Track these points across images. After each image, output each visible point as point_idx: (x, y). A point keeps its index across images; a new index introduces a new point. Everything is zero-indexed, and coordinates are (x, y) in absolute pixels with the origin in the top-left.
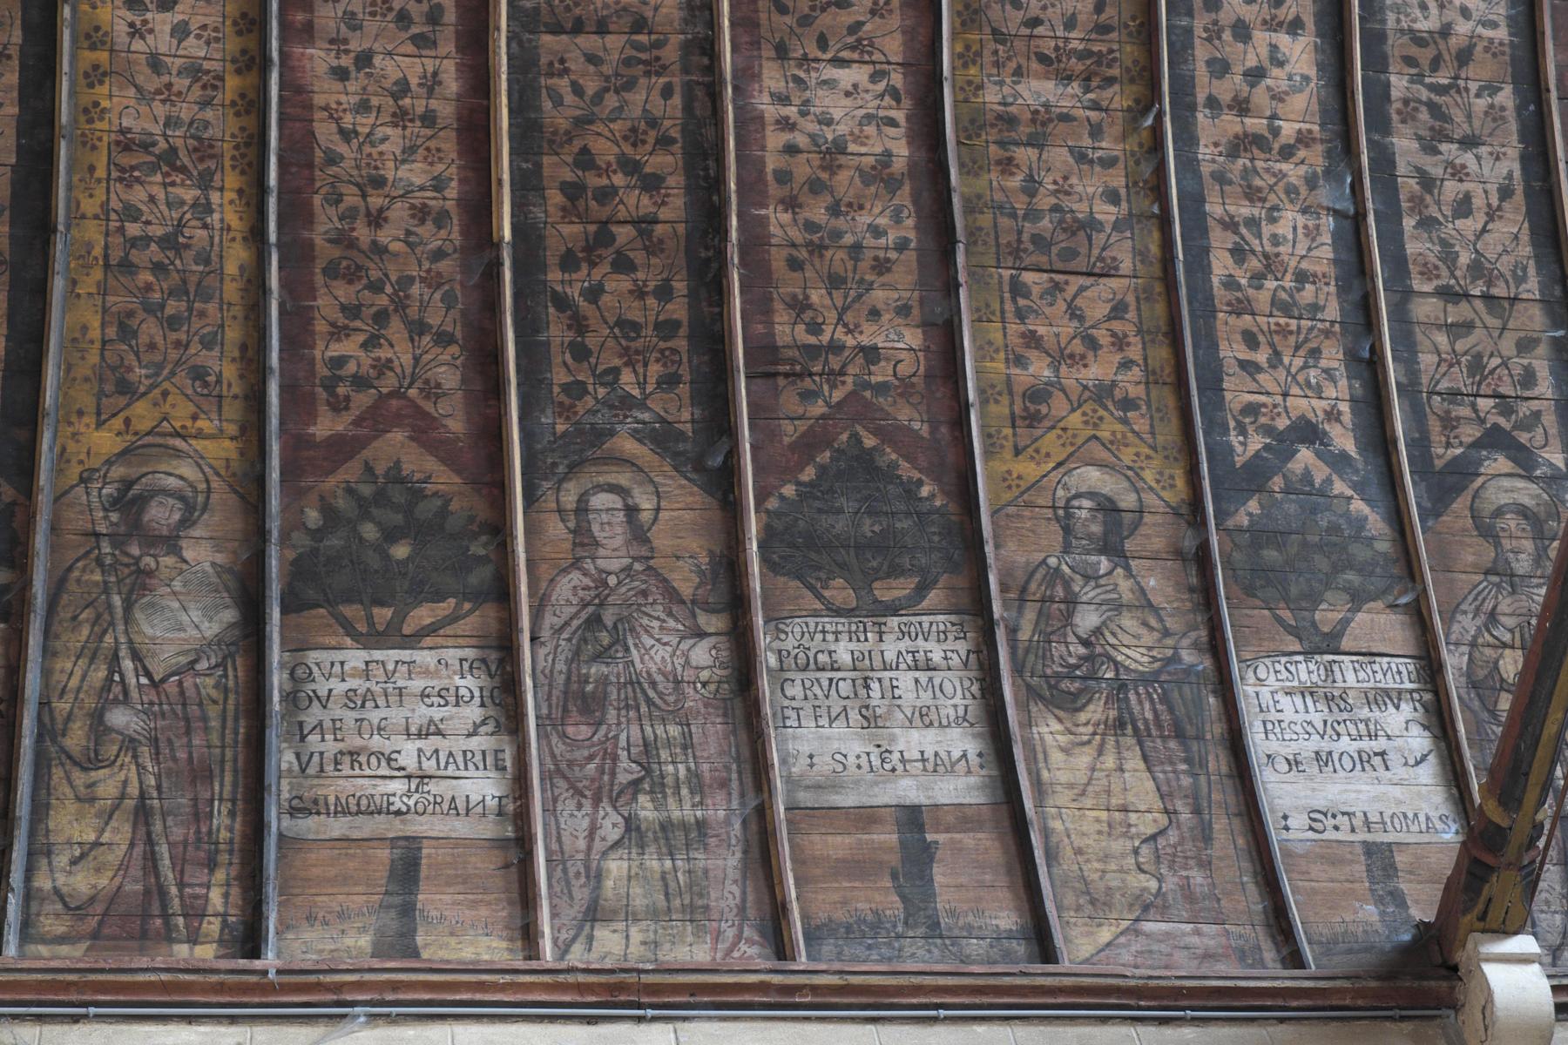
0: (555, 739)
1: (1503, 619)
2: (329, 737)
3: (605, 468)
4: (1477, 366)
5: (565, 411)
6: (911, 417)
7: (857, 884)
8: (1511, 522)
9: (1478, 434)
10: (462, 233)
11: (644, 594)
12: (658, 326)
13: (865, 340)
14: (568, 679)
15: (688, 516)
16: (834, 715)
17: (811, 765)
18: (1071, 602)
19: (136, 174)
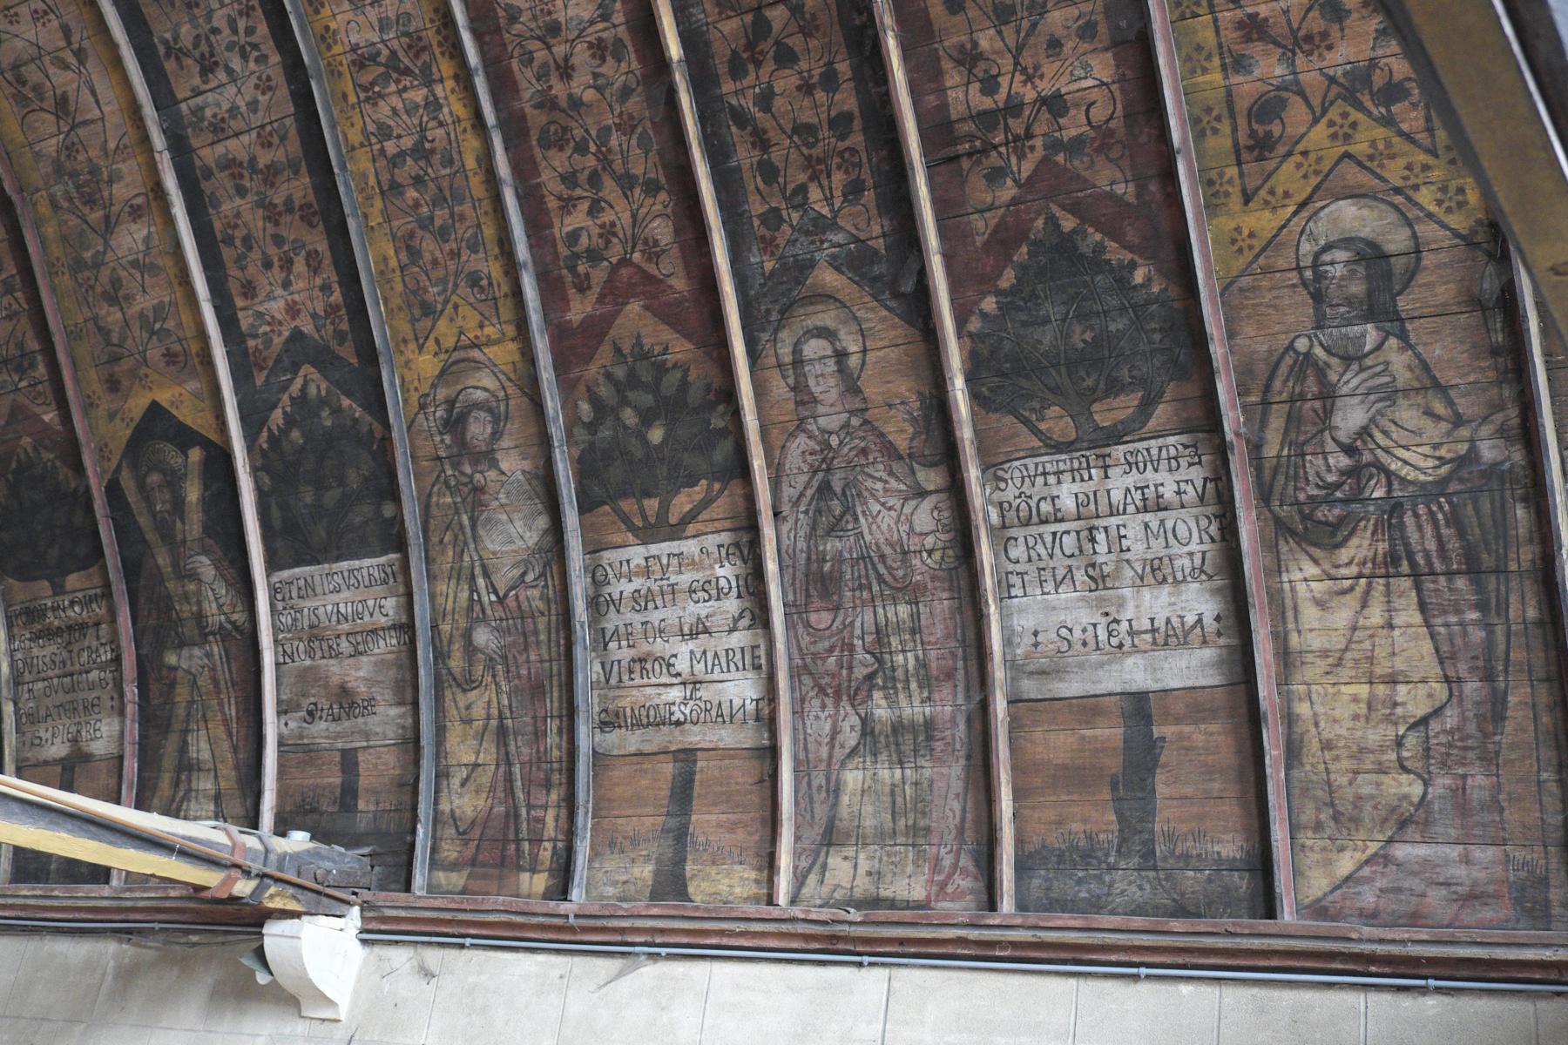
0: (801, 630)
2: (624, 643)
3: (811, 309)
5: (768, 245)
6: (1113, 180)
7: (1075, 797)
10: (639, 60)
11: (864, 452)
12: (832, 123)
13: (1045, 87)
14: (809, 558)
15: (893, 354)
16: (1059, 578)
17: (1036, 645)
18: (1328, 396)
19: (377, 89)
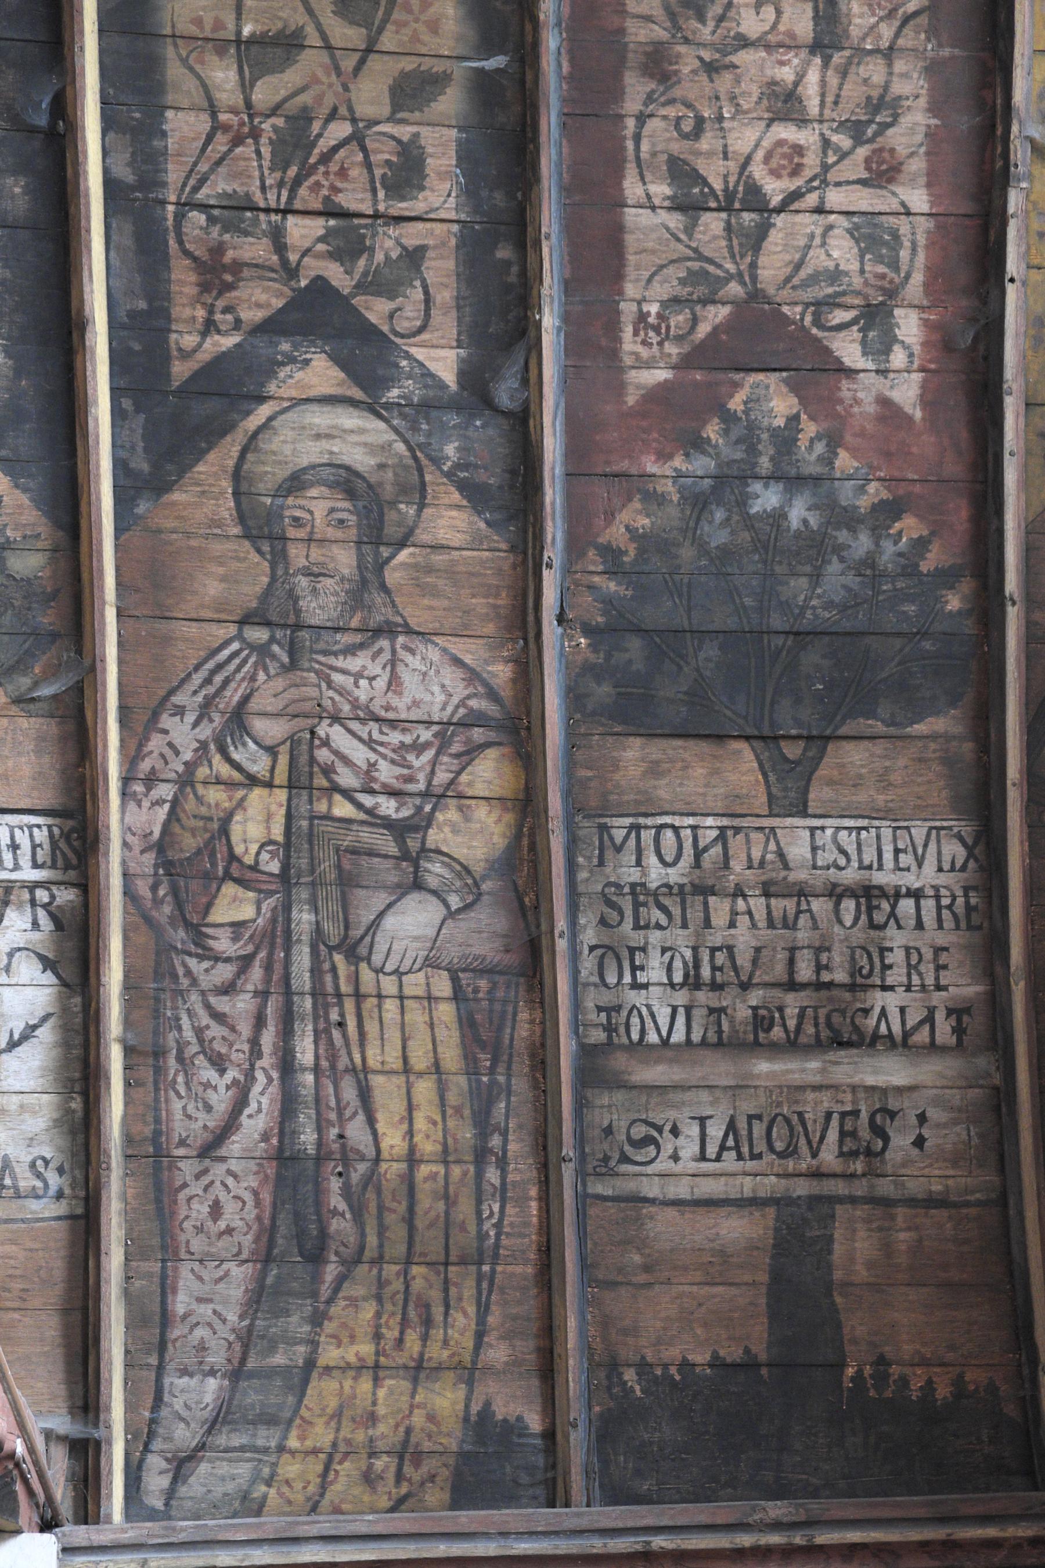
1: (259, 725)
4: (295, 143)
8: (319, 505)
9: (278, 303)
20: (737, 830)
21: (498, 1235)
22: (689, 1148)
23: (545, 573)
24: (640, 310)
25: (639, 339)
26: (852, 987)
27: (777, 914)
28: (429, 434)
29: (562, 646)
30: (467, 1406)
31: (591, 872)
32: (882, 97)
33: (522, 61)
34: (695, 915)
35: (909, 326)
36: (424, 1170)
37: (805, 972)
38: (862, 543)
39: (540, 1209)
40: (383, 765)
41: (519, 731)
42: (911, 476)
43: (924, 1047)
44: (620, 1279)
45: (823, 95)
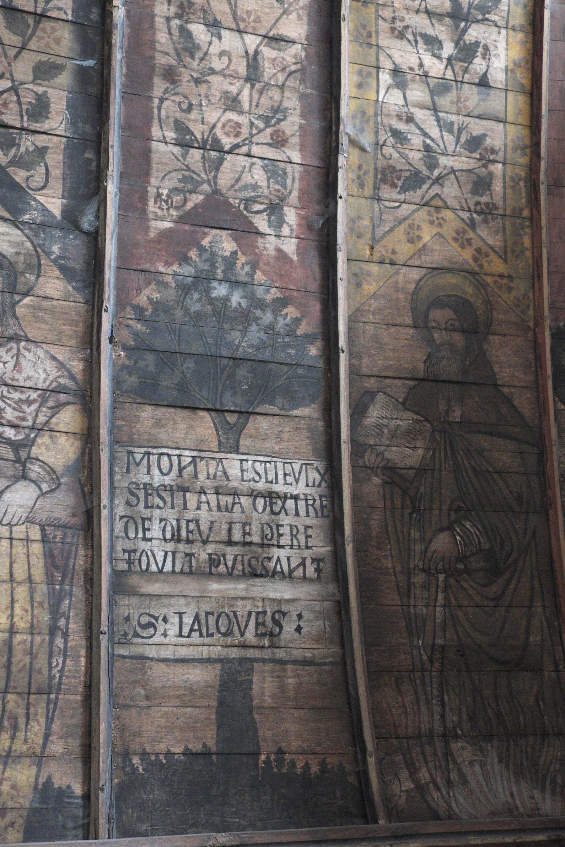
20: (202, 458)
21: (61, 677)
22: (173, 630)
23: (104, 314)
24: (158, 192)
25: (157, 206)
26: (262, 545)
27: (223, 504)
28: (45, 240)
29: (111, 355)
30: (37, 779)
31: (122, 476)
32: (279, 107)
33: (102, 64)
34: (179, 502)
35: (291, 216)
36: (18, 638)
37: (237, 536)
38: (267, 317)
39: (86, 662)
40: (8, 410)
41: (87, 397)
42: (291, 287)
43: (300, 579)
44: (132, 703)
45: (251, 101)
